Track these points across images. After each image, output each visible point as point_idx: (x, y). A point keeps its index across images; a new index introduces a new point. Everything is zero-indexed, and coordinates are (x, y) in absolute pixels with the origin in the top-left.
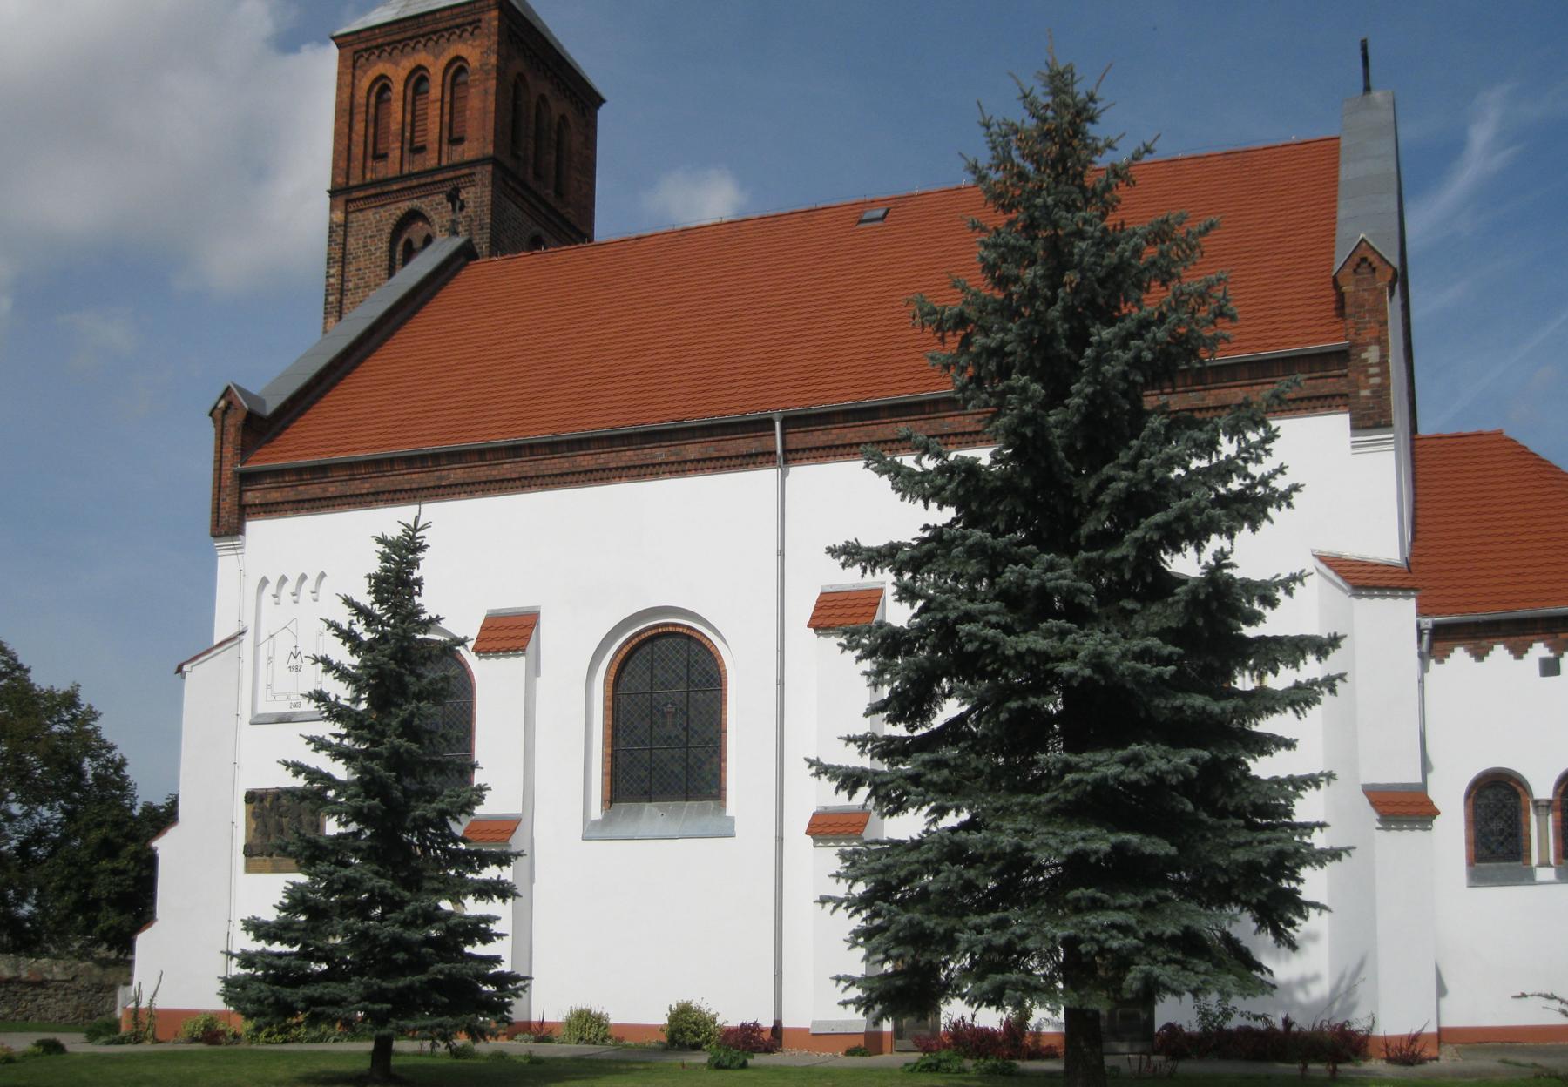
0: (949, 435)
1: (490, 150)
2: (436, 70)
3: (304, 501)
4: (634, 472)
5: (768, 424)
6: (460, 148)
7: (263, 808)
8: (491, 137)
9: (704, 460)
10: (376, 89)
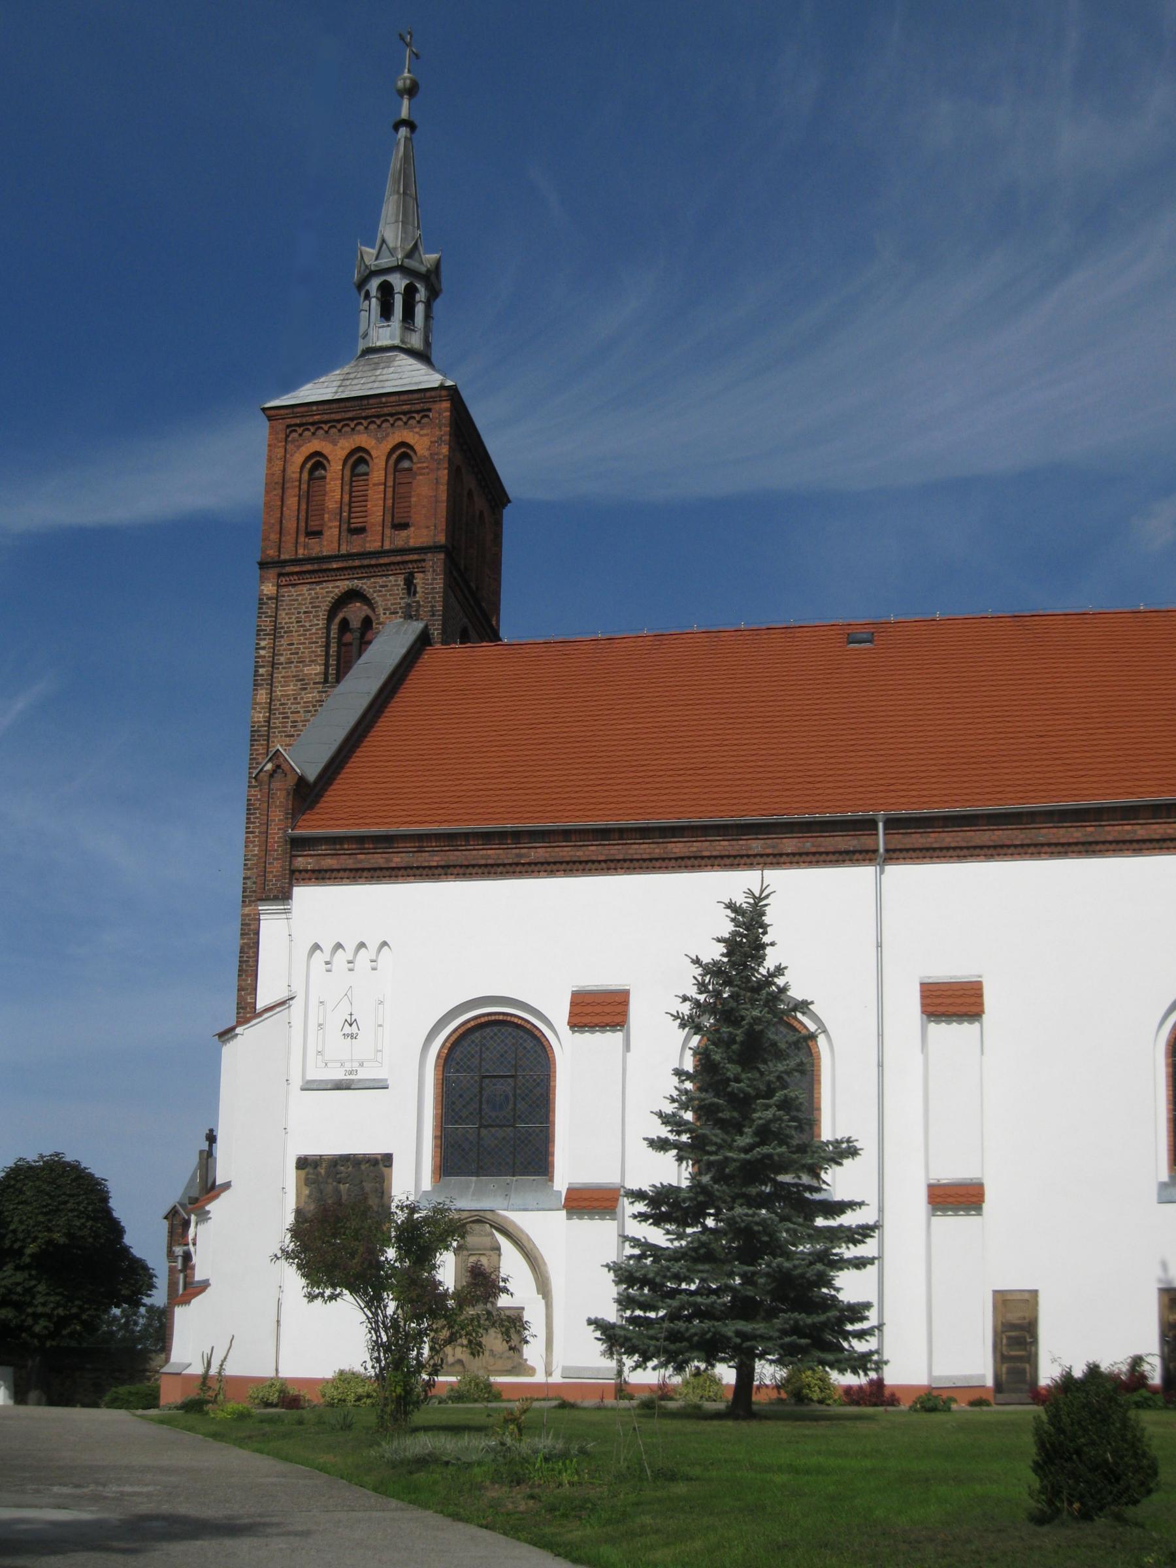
0: (1043, 845)
1: (442, 539)
2: (379, 447)
3: (363, 870)
4: (728, 861)
5: (871, 824)
6: (404, 533)
7: (318, 1174)
8: (442, 525)
9: (801, 854)
10: (309, 466)
